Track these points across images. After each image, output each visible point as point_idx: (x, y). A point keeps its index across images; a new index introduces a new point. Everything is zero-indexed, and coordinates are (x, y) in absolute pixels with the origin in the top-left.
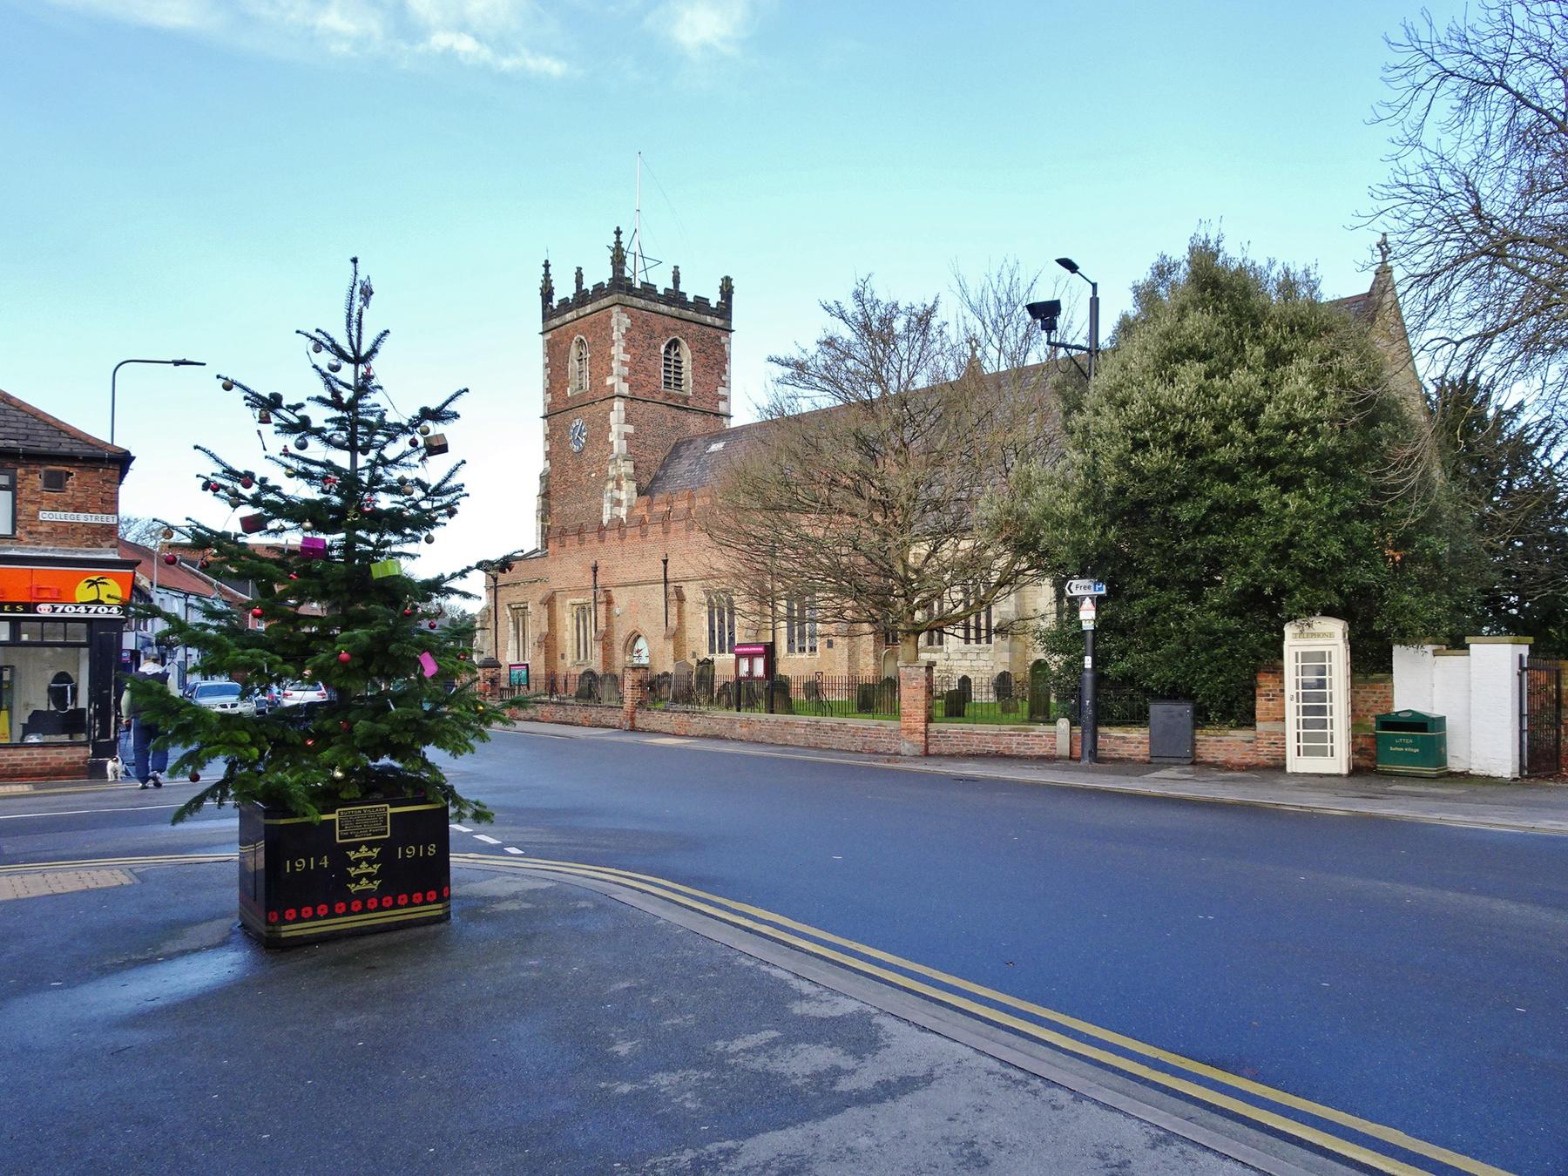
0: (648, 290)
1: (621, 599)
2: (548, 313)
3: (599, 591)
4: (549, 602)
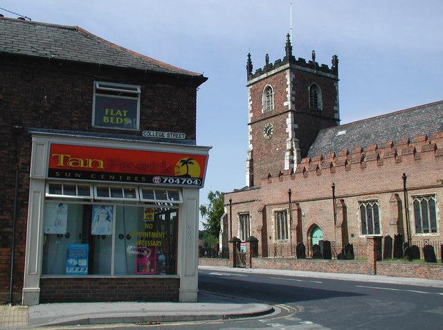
1: (305, 208)
2: (250, 76)
3: (338, 201)
4: (264, 211)
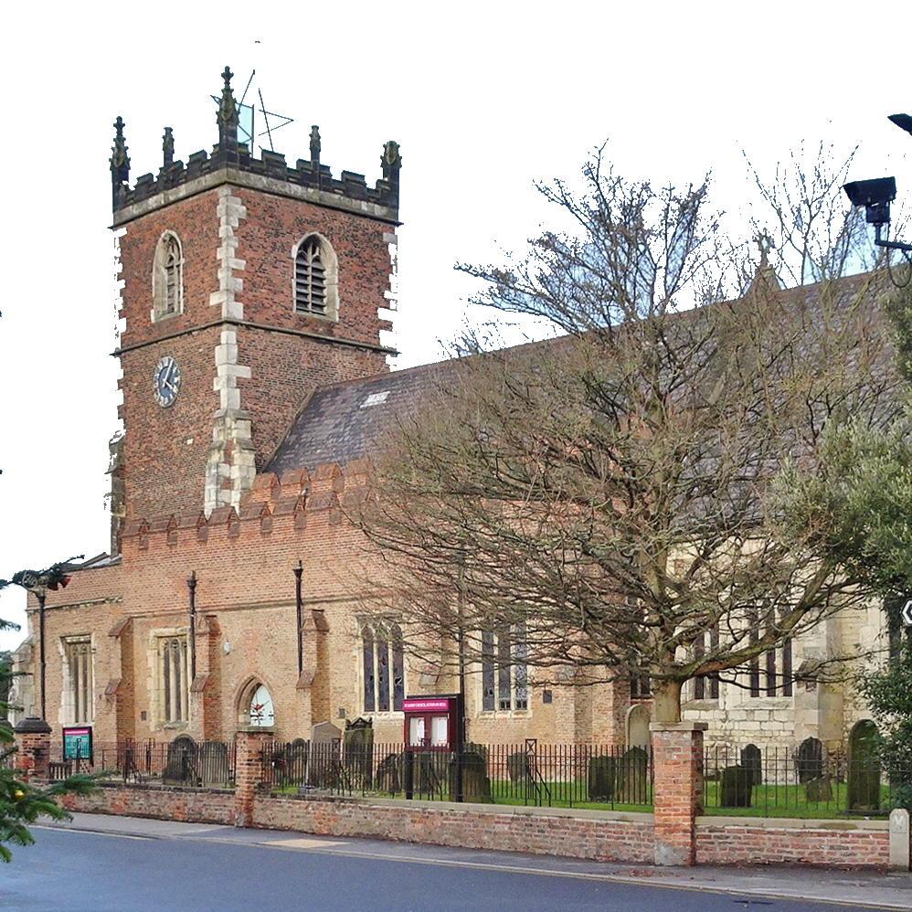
0: (273, 162)
1: (233, 628)
2: (122, 198)
4: (124, 634)
